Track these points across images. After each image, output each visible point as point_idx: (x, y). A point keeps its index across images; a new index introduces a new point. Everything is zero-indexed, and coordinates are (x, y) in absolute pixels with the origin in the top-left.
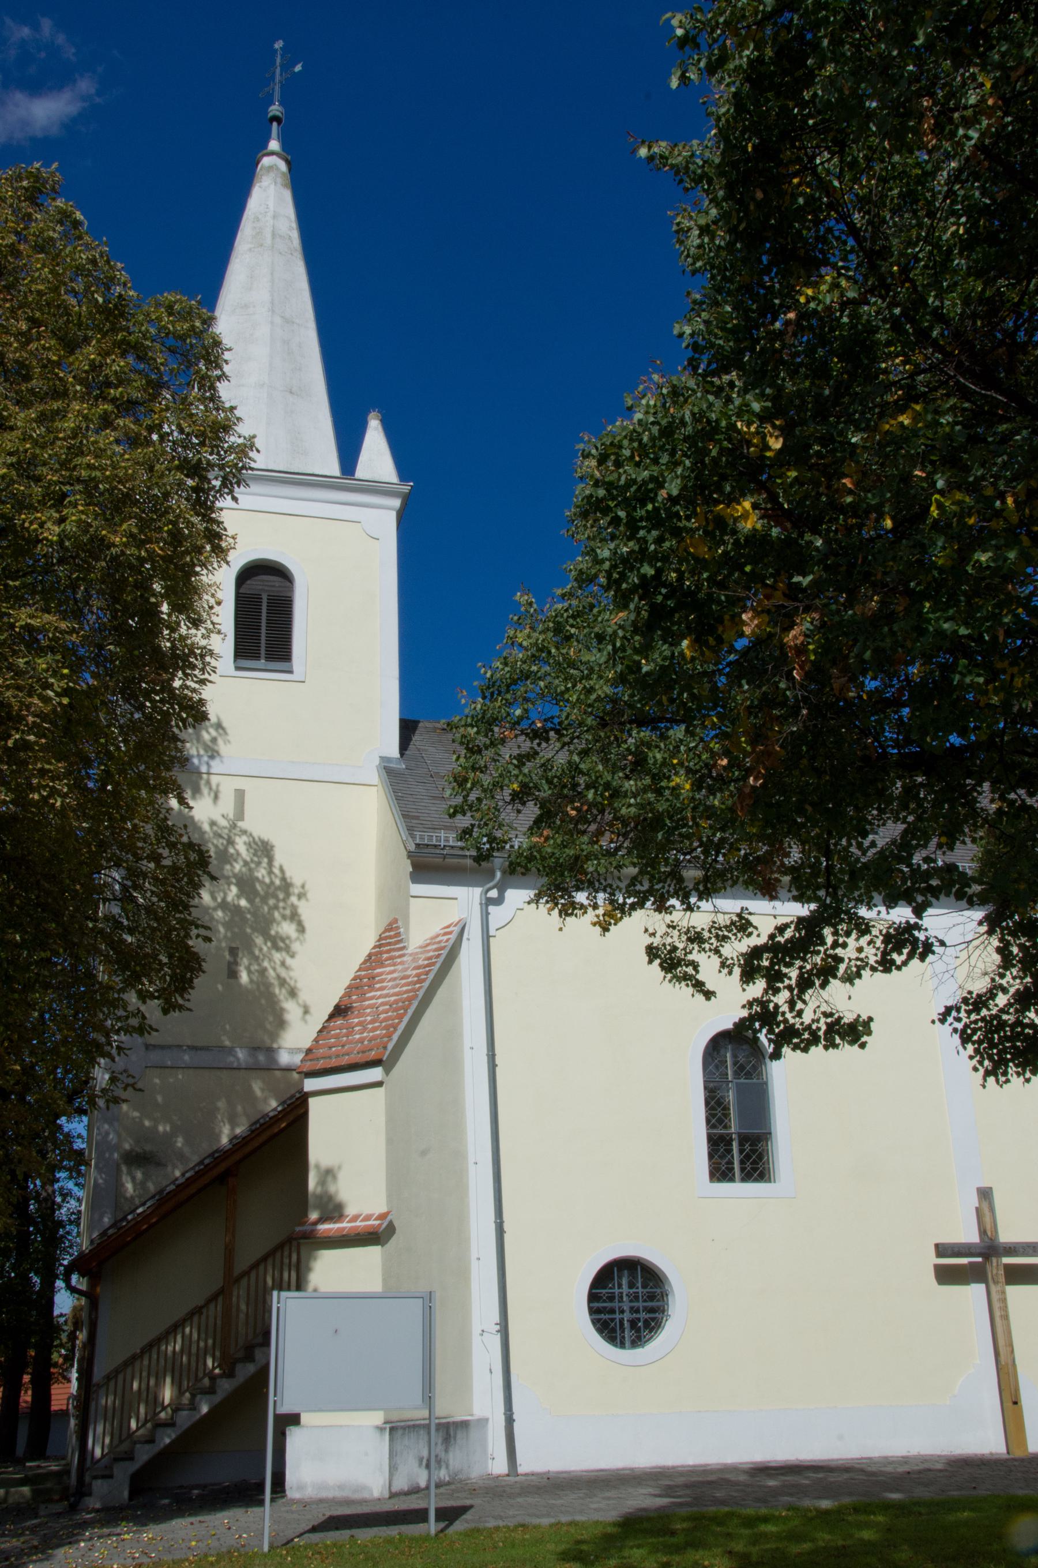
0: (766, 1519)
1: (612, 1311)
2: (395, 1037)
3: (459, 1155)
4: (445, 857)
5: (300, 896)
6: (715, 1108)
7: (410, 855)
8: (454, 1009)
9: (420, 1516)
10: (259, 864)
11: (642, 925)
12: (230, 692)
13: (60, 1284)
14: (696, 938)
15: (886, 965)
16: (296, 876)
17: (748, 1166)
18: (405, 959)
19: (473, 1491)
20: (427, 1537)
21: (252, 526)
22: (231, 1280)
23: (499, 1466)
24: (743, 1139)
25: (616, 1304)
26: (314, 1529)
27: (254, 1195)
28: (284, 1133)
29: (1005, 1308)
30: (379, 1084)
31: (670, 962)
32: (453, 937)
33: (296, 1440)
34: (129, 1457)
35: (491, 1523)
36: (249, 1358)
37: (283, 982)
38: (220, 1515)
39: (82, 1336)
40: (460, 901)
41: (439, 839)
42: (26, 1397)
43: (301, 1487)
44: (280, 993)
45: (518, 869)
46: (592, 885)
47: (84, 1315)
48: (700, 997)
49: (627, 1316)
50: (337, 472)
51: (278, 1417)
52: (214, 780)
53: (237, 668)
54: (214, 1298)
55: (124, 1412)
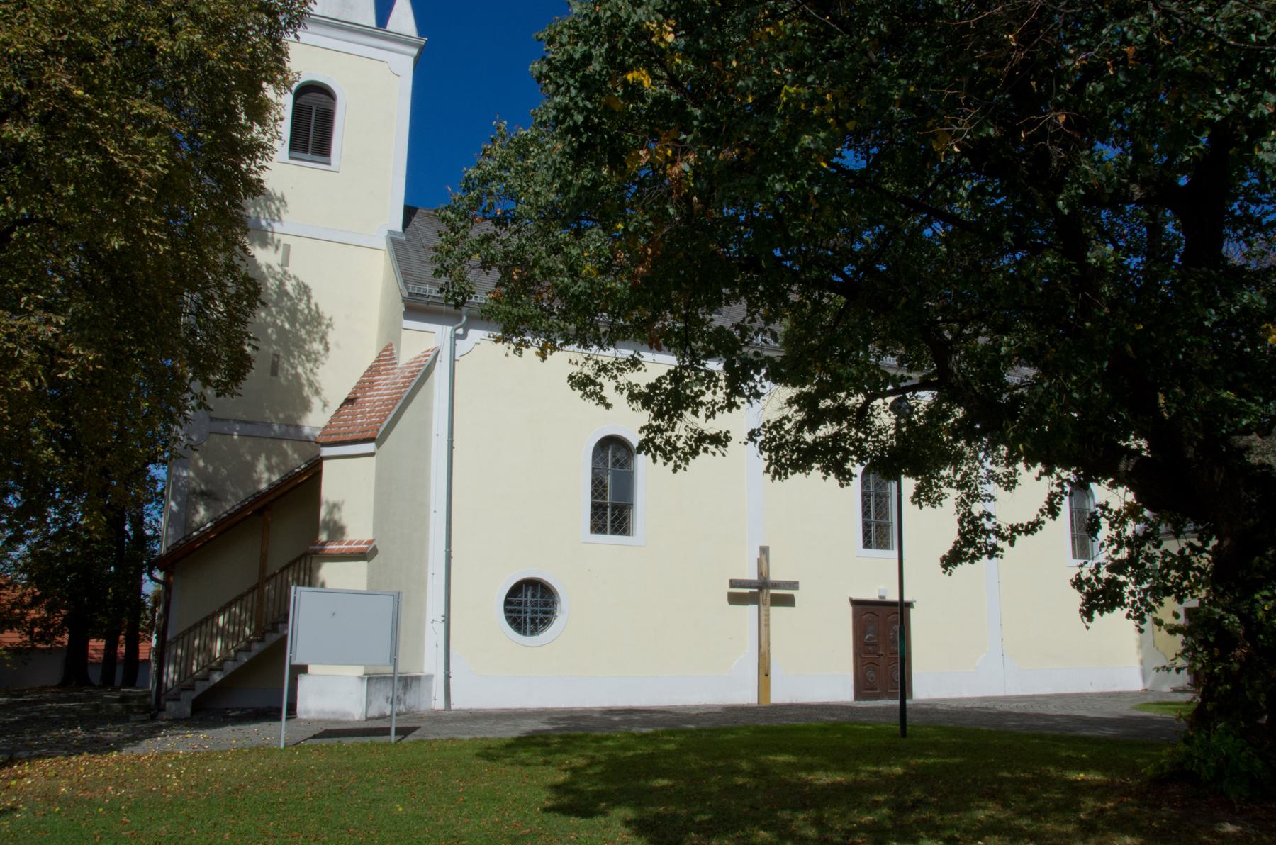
0: (607, 738)
1: (520, 612)
2: (385, 423)
3: (425, 506)
4: (428, 303)
5: (328, 326)
6: (598, 486)
7: (404, 300)
8: (428, 408)
9: (386, 731)
10: (300, 300)
11: (568, 360)
12: (280, 171)
13: (145, 576)
14: (603, 369)
15: (731, 406)
16: (326, 311)
17: (616, 524)
19: (421, 718)
20: (389, 744)
21: (307, 56)
22: (264, 579)
23: (439, 704)
24: (615, 507)
25: (522, 608)
26: (315, 737)
27: (282, 524)
28: (302, 487)
29: (768, 620)
30: (372, 454)
31: (581, 383)
32: (430, 359)
33: (304, 683)
34: (191, 688)
35: (432, 737)
36: (275, 630)
37: (311, 384)
38: (252, 726)
39: (159, 610)
40: (435, 335)
41: (425, 290)
42: (122, 649)
43: (307, 712)
44: (307, 391)
45: (484, 317)
46: (536, 332)
47: (162, 595)
48: (602, 407)
49: (529, 615)
50: (374, 25)
51: (292, 667)
52: (276, 236)
53: (291, 158)
54: (254, 589)
55: (188, 660)
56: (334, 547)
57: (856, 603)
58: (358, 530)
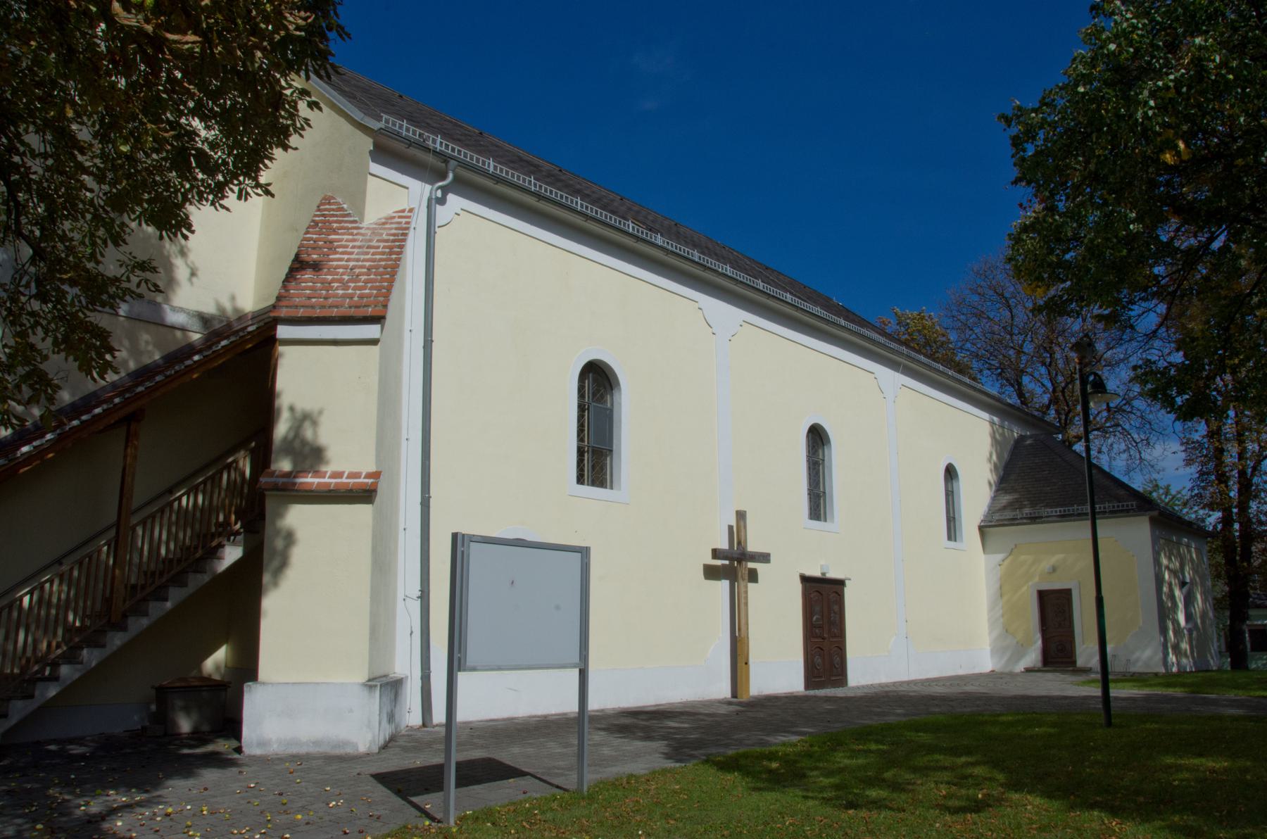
18: (362, 231)
30: (374, 342)
43: (262, 744)
56: (310, 480)
57: (805, 579)
58: (346, 457)
